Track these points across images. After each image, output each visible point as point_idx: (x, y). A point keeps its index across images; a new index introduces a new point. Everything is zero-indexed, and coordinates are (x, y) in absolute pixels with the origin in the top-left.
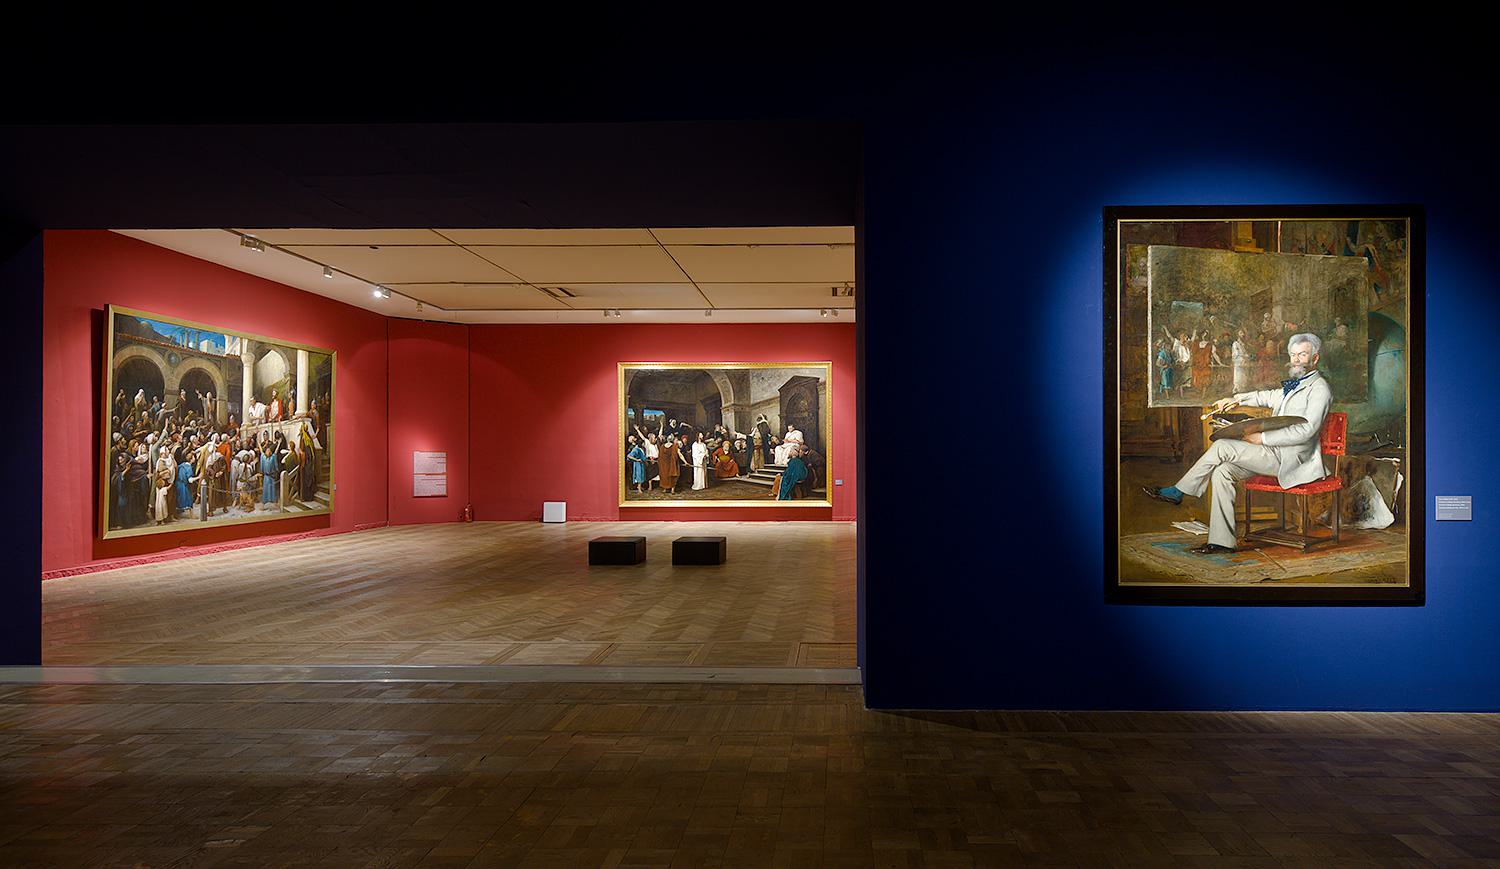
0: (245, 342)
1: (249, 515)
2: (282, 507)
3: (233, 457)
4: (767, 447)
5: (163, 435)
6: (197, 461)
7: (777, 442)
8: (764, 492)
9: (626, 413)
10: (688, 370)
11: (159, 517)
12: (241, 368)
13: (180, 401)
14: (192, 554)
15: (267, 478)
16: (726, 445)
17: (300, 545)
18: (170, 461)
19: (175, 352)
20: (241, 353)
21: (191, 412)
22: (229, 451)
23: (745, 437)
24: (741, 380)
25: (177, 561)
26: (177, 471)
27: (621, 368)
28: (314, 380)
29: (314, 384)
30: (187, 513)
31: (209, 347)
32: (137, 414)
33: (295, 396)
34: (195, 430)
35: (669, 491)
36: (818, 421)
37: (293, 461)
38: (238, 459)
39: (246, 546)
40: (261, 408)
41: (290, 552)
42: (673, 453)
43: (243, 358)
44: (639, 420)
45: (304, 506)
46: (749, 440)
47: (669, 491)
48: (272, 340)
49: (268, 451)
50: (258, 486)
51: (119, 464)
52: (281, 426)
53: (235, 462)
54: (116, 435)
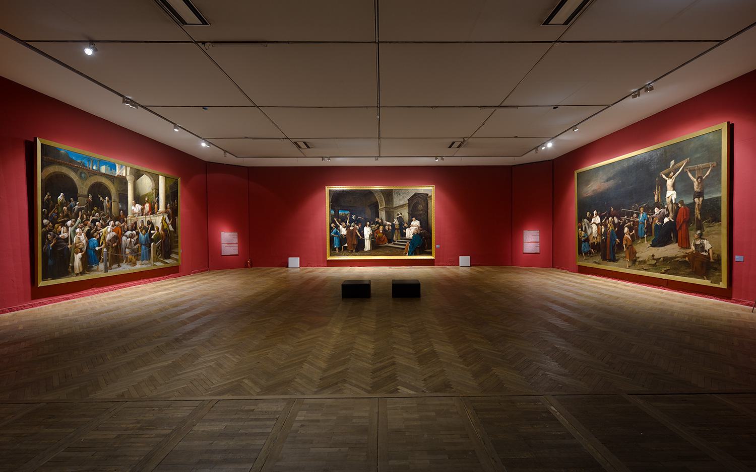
0: (129, 169)
1: (133, 268)
2: (152, 263)
3: (123, 235)
4: (402, 229)
5: (78, 221)
6: (100, 237)
7: (407, 226)
8: (400, 252)
9: (330, 212)
10: (361, 190)
11: (77, 271)
12: (126, 183)
13: (89, 201)
14: (99, 292)
15: (143, 247)
16: (381, 228)
17: (163, 284)
18: (83, 237)
19: (85, 171)
20: (126, 175)
21: (96, 208)
22: (120, 232)
23: (391, 224)
24: (388, 195)
25: (89, 297)
26: (88, 243)
27: (327, 189)
28: (169, 192)
29: (168, 195)
30: (95, 268)
31: (106, 169)
32: (60, 208)
33: (158, 201)
34: (99, 219)
35: (352, 251)
36: (428, 215)
37: (158, 237)
38: (126, 236)
39: (132, 285)
40: (138, 207)
41: (158, 289)
42: (354, 234)
43: (128, 178)
44: (336, 215)
45: (164, 262)
46: (393, 225)
47: (352, 251)
48: (144, 169)
49: (144, 232)
50: (138, 251)
51: (48, 239)
52: (150, 218)
53: (124, 238)
54: (45, 221)
